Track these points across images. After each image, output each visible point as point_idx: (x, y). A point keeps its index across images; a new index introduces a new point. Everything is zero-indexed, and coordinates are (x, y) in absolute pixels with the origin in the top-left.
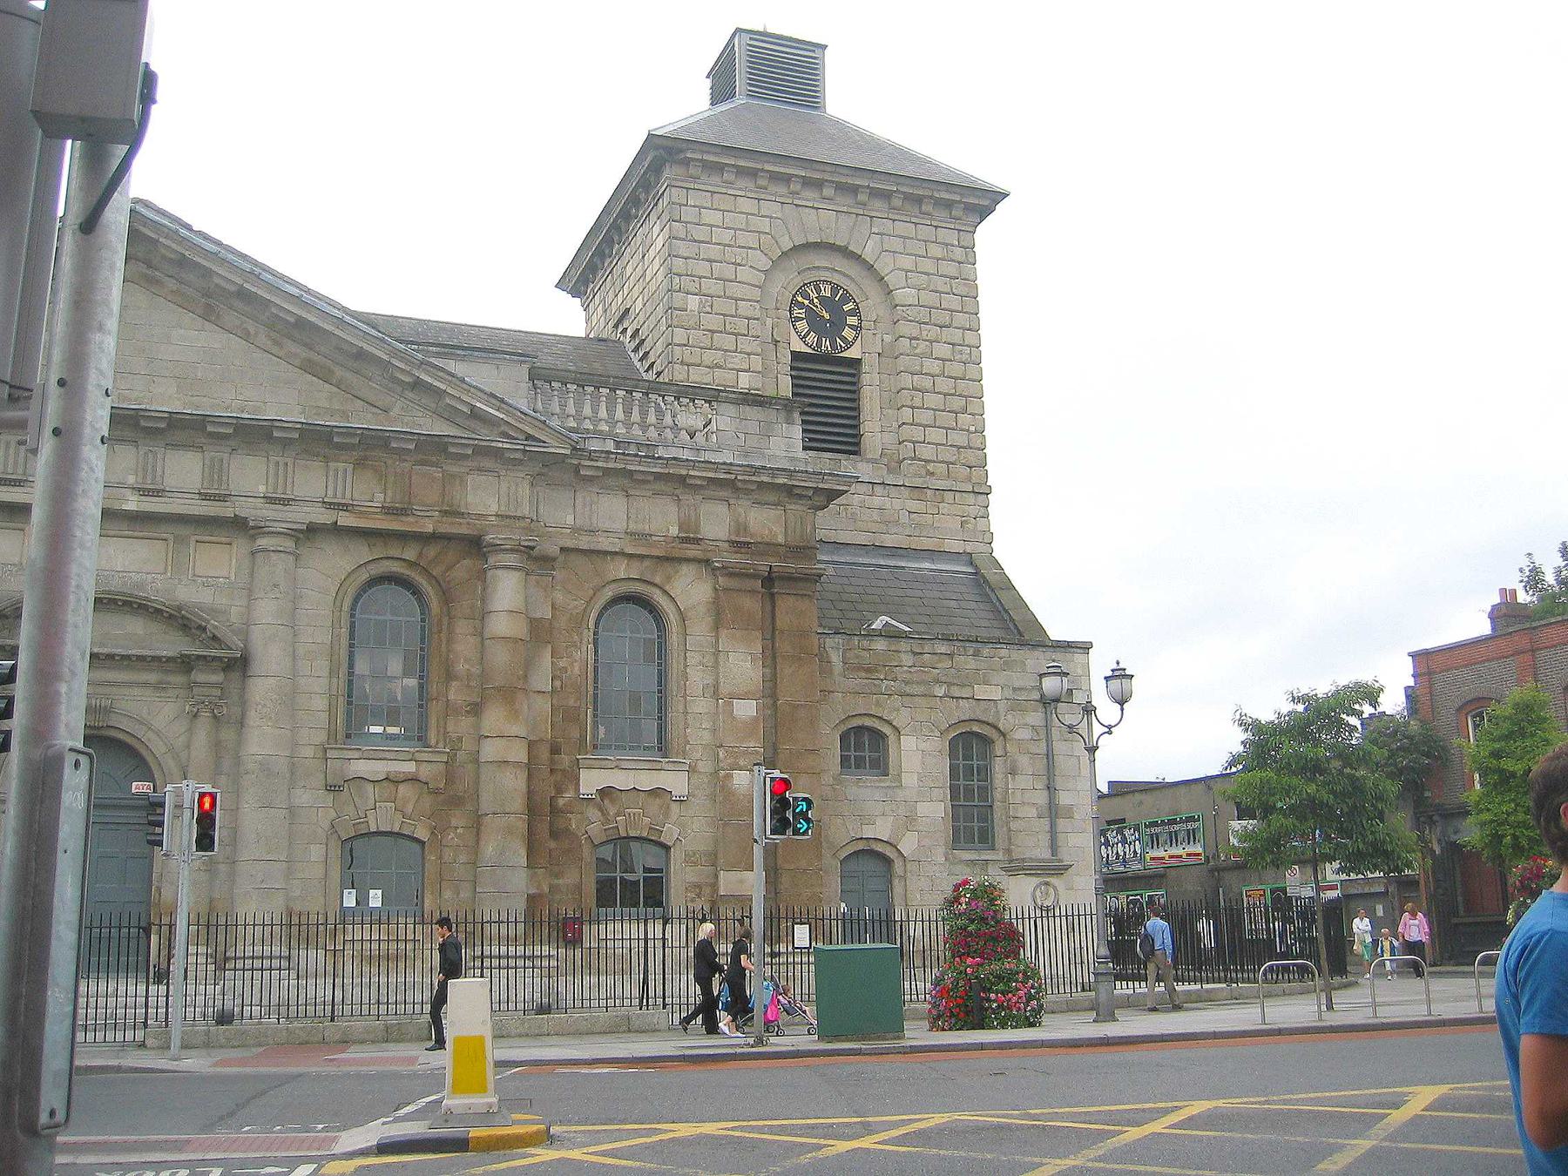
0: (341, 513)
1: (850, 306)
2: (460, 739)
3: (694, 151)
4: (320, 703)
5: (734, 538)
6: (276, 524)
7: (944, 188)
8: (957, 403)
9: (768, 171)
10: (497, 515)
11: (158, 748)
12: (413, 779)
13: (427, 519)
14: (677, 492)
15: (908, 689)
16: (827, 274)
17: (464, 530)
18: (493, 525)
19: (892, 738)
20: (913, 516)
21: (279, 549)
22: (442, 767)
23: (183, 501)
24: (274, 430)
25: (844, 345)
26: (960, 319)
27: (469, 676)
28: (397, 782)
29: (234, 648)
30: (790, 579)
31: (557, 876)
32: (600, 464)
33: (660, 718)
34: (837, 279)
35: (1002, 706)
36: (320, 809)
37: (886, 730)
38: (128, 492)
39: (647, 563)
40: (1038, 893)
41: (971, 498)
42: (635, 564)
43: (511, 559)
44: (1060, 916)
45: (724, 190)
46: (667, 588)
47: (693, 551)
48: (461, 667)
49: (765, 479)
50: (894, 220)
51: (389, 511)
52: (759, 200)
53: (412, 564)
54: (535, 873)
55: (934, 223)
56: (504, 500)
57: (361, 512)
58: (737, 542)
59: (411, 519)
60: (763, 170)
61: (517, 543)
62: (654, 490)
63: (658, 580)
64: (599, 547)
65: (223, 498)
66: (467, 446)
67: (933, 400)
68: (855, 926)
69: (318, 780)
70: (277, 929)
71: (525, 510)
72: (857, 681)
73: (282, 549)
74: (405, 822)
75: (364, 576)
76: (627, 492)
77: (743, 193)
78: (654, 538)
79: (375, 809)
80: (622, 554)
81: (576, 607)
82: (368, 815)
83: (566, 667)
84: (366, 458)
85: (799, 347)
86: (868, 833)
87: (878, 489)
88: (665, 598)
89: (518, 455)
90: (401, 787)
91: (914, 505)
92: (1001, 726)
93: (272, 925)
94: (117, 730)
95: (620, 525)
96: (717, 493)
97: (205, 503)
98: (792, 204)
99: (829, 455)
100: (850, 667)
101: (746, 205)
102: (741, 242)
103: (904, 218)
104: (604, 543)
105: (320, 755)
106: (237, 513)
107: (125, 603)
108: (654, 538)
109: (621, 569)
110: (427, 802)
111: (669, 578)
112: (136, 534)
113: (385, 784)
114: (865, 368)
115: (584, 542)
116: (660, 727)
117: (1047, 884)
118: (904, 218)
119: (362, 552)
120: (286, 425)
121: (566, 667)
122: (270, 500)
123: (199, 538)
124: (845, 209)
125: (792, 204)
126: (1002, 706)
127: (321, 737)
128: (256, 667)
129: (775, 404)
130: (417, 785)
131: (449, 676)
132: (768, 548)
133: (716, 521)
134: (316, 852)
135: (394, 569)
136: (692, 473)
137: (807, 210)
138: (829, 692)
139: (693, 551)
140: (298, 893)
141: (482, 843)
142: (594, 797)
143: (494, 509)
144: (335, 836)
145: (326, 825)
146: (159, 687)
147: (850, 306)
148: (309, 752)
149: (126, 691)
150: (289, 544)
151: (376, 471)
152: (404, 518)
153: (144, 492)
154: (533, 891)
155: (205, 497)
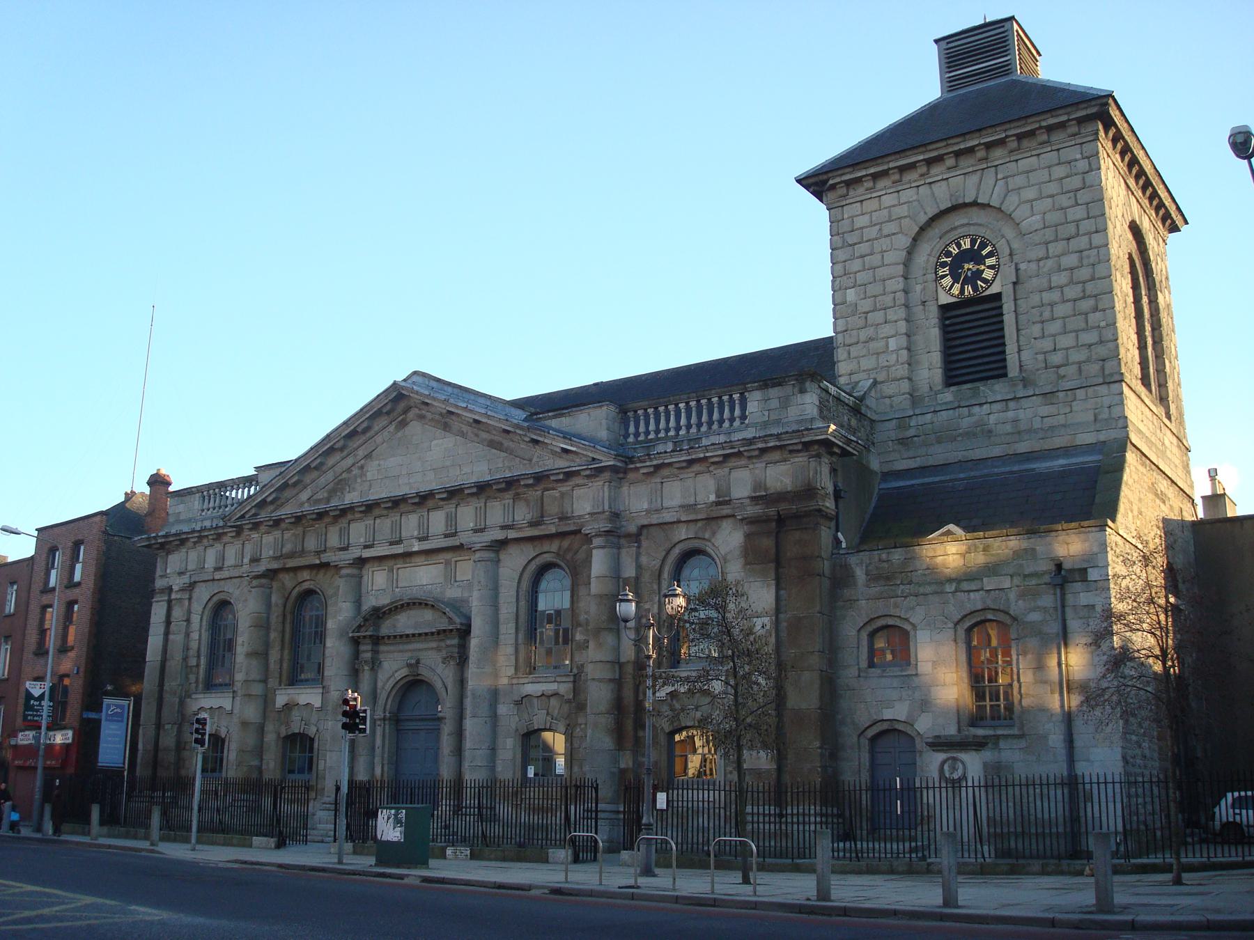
1: (989, 249)
3: (834, 177)
5: (754, 495)
7: (1049, 115)
8: (1086, 305)
9: (984, 144)
12: (556, 694)
15: (921, 590)
16: (965, 229)
19: (912, 633)
20: (1045, 420)
22: (571, 685)
25: (984, 285)
26: (1086, 226)
28: (549, 697)
30: (797, 517)
32: (648, 464)
34: (972, 230)
35: (1012, 596)
37: (907, 627)
39: (700, 524)
40: (946, 767)
41: (1103, 390)
42: (692, 526)
44: (752, 792)
45: (869, 196)
47: (726, 510)
49: (761, 445)
50: (1017, 161)
51: (533, 524)
52: (898, 192)
55: (1054, 148)
57: (520, 528)
58: (755, 497)
59: (543, 527)
60: (889, 169)
63: (707, 536)
64: (664, 521)
66: (558, 474)
67: (1061, 310)
70: (1118, 786)
72: (875, 590)
77: (884, 192)
78: (699, 507)
80: (679, 522)
81: (655, 565)
84: (518, 494)
85: (945, 299)
86: (887, 714)
87: (1012, 404)
91: (1044, 410)
92: (1012, 612)
93: (1113, 783)
95: (676, 502)
96: (739, 463)
98: (925, 184)
99: (969, 386)
100: (873, 578)
101: (888, 200)
102: (885, 232)
103: (1025, 155)
104: (668, 517)
108: (699, 507)
109: (682, 533)
110: (566, 707)
111: (714, 533)
112: (430, 562)
114: (1004, 299)
115: (655, 519)
117: (954, 759)
118: (1025, 155)
119: (529, 551)
122: (476, 531)
123: (456, 559)
124: (971, 169)
125: (925, 184)
126: (1012, 596)
129: (789, 381)
132: (780, 497)
133: (742, 483)
135: (549, 559)
136: (707, 455)
137: (939, 184)
138: (855, 601)
139: (726, 510)
143: (588, 509)
147: (989, 249)
152: (540, 527)
153: (420, 539)
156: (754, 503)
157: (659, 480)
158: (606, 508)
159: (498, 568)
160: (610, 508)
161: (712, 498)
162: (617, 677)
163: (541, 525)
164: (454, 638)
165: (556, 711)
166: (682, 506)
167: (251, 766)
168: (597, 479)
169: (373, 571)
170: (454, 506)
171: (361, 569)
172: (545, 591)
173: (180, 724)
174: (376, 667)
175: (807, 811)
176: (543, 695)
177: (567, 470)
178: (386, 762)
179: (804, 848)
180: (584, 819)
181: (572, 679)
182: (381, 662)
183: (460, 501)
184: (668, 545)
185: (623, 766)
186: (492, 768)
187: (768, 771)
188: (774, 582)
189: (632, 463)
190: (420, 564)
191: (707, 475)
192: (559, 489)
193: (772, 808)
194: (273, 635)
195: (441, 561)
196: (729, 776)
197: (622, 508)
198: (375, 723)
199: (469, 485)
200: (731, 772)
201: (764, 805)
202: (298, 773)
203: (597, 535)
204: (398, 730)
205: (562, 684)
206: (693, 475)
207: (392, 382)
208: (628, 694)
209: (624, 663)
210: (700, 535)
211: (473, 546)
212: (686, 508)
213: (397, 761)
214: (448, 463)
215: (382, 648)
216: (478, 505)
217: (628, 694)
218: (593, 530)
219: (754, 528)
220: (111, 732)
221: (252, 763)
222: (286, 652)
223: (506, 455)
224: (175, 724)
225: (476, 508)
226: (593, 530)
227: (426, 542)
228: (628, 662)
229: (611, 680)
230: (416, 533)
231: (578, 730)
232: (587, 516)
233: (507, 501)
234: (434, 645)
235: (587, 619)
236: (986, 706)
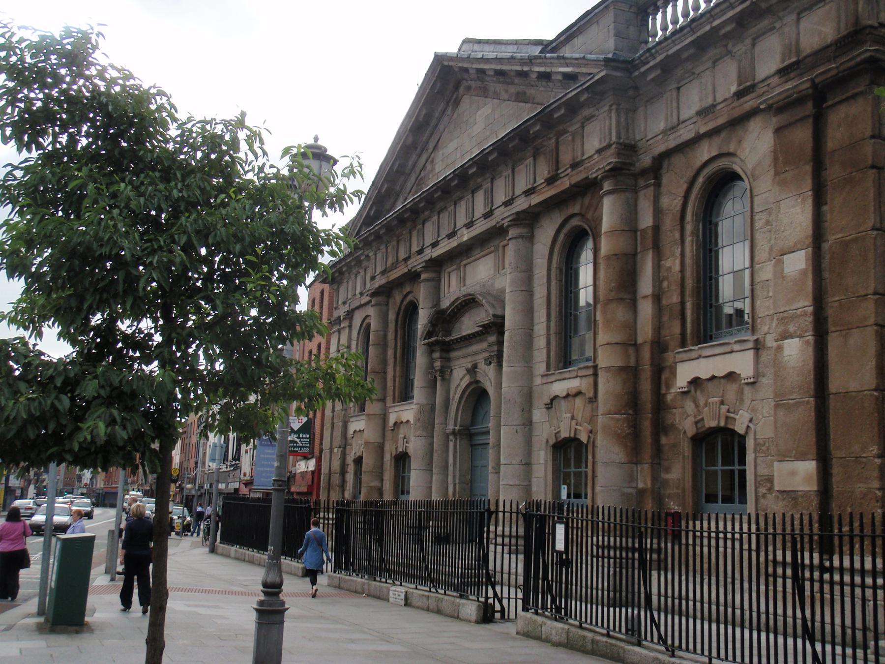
12: (579, 393)
32: (651, 64)
51: (551, 181)
59: (559, 182)
109: (705, 152)
132: (821, 54)
136: (715, 23)
156: (783, 79)
157: (674, 86)
158: (614, 139)
159: (532, 244)
160: (619, 136)
162: (632, 363)
163: (557, 180)
165: (580, 415)
166: (699, 113)
167: (371, 487)
169: (449, 273)
170: (489, 180)
171: (439, 273)
172: (805, 314)
173: (345, 448)
174: (447, 377)
175: (857, 565)
177: (565, 99)
178: (457, 481)
179: (853, 628)
180: (592, 557)
181: (591, 372)
182: (451, 371)
184: (690, 174)
185: (641, 485)
186: (528, 489)
187: (806, 494)
188: (810, 193)
189: (636, 68)
191: (728, 59)
192: (570, 129)
193: (816, 556)
194: (390, 353)
196: (762, 501)
197: (638, 137)
198: (448, 438)
200: (764, 496)
202: (723, 502)
203: (604, 178)
204: (472, 446)
207: (433, 56)
208: (646, 386)
209: (641, 344)
210: (725, 150)
212: (705, 112)
213: (471, 481)
214: (488, 133)
215: (454, 354)
217: (646, 386)
218: (600, 172)
219: (784, 118)
220: (266, 456)
221: (372, 484)
222: (398, 368)
223: (530, 105)
224: (340, 447)
226: (600, 172)
228: (646, 342)
229: (622, 369)
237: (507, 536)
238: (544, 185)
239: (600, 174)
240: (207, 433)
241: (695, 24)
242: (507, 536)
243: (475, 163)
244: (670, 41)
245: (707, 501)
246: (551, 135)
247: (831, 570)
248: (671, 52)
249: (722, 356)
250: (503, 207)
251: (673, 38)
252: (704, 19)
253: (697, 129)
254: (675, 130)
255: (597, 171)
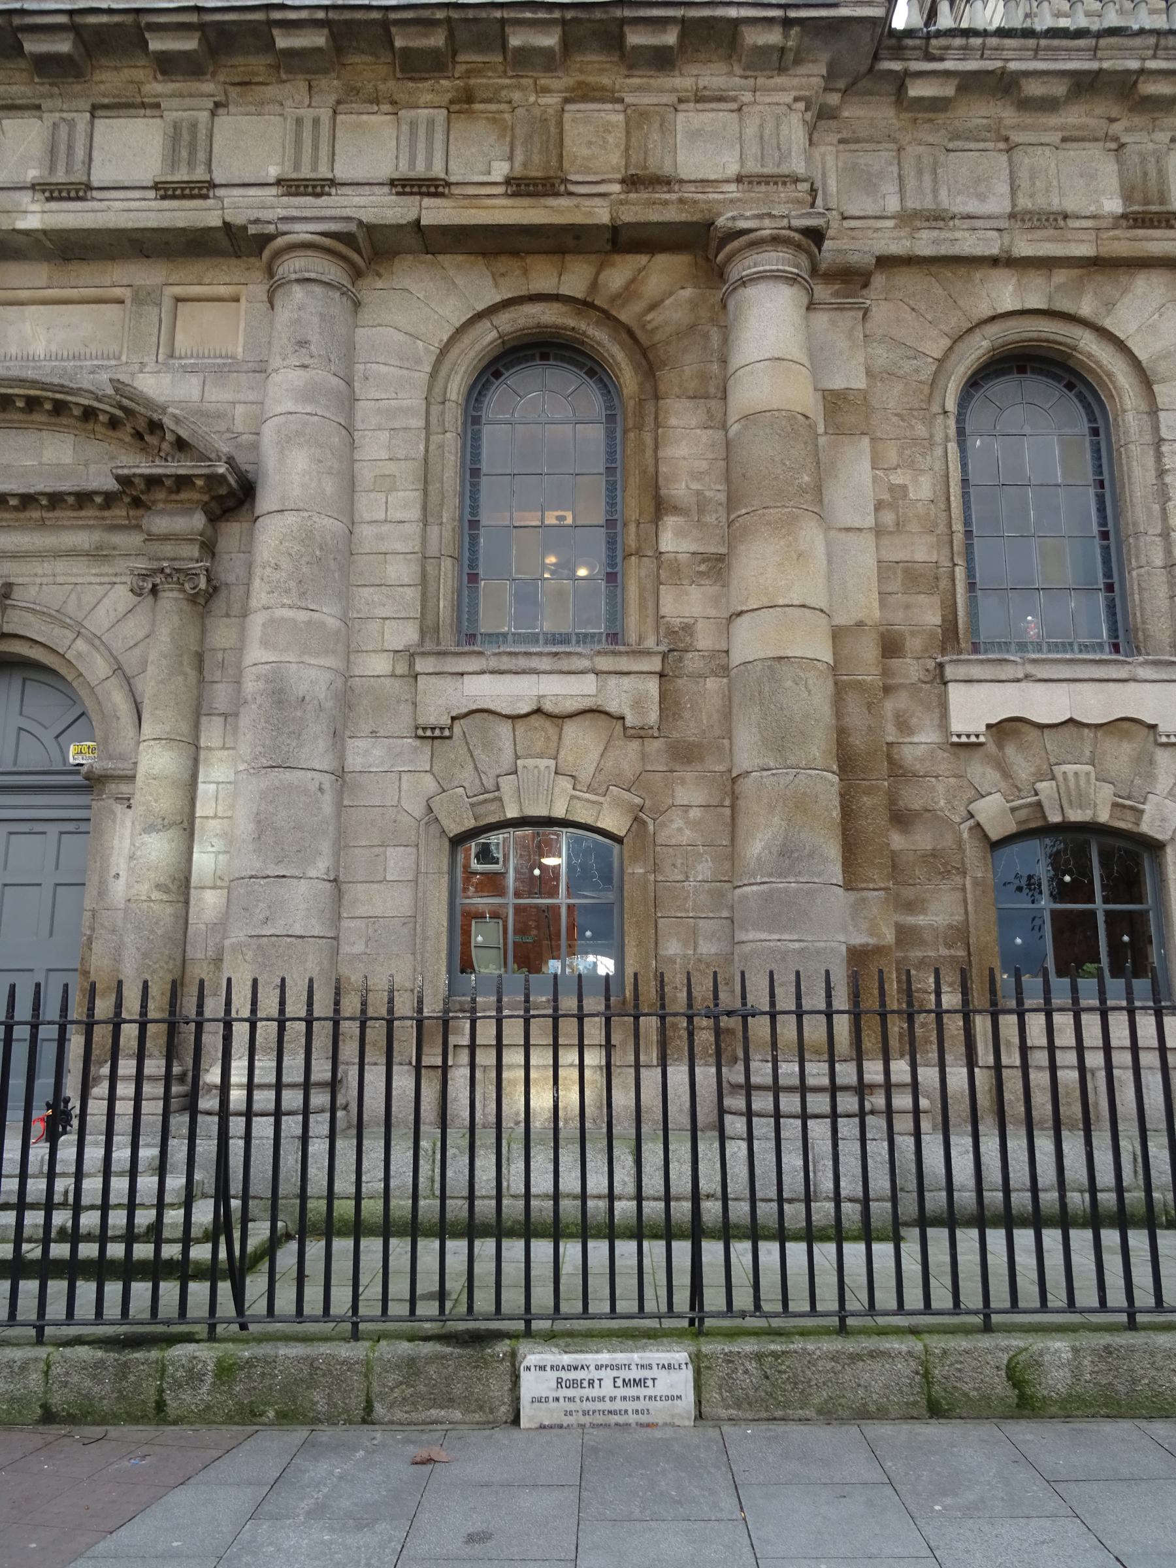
0: (427, 201)
2: (688, 629)
4: (401, 571)
6: (297, 227)
10: (739, 179)
11: (97, 668)
13: (598, 201)
14: (1116, 128)
17: (673, 215)
18: (731, 201)
21: (307, 275)
23: (126, 204)
24: (276, 32)
27: (702, 505)
28: (559, 718)
29: (213, 456)
31: (910, 906)
32: (948, 65)
33: (1110, 588)
36: (405, 777)
38: (25, 198)
39: (1061, 276)
43: (776, 260)
46: (1108, 323)
48: (680, 489)
53: (583, 305)
54: (864, 900)
56: (753, 149)
59: (563, 202)
61: (785, 222)
62: (1062, 128)
63: (1086, 308)
65: (201, 190)
68: (76, 1043)
69: (402, 722)
71: (798, 166)
73: (313, 275)
74: (578, 798)
75: (486, 337)
76: (1007, 139)
79: (516, 772)
82: (502, 785)
83: (906, 486)
88: (1104, 344)
89: (773, 37)
90: (571, 730)
94: (23, 642)
97: (167, 204)
104: (969, 243)
105: (402, 669)
106: (228, 219)
107: (33, 404)
111: (1110, 305)
113: (535, 721)
115: (925, 243)
116: (1111, 607)
120: (293, 15)
121: (906, 486)
122: (290, 186)
123: (178, 290)
127: (406, 635)
128: (267, 500)
130: (602, 721)
131: (659, 507)
134: (398, 861)
136: (1152, 65)
140: (359, 948)
141: (739, 841)
142: (982, 739)
143: (733, 169)
144: (434, 828)
145: (418, 810)
146: (98, 555)
148: (380, 665)
149: (39, 568)
150: (333, 271)
151: (494, 121)
153: (54, 192)
154: (860, 939)
155: (166, 191)
161: (1113, 205)
163: (557, 194)
164: (188, 512)
168: (779, 80)
176: (538, 711)
183: (234, 92)
190: (24, 294)
195: (118, 292)
199: (304, 15)
201: (52, 1137)
205: (613, 681)
206: (1055, 138)
211: (283, 227)
216: (307, 114)
225: (299, 122)
226: (767, 222)
227: (78, 205)
230: (33, 174)
231: (678, 823)
232: (733, 187)
233: (424, 113)
234: (81, 539)
235: (698, 493)
236: (1106, 900)
237: (790, 1089)
238: (500, 190)
239: (767, 228)
240: (880, 71)
241: (1113, 40)
242: (790, 1089)
243: (201, 27)
244: (1031, 42)
245: (462, 972)
246: (555, 84)
247: (748, 1088)
248: (1013, 66)
249: (1098, 685)
250: (274, 191)
251: (1043, 42)
252: (1138, 42)
253: (1006, 243)
254: (941, 224)
255: (760, 217)
